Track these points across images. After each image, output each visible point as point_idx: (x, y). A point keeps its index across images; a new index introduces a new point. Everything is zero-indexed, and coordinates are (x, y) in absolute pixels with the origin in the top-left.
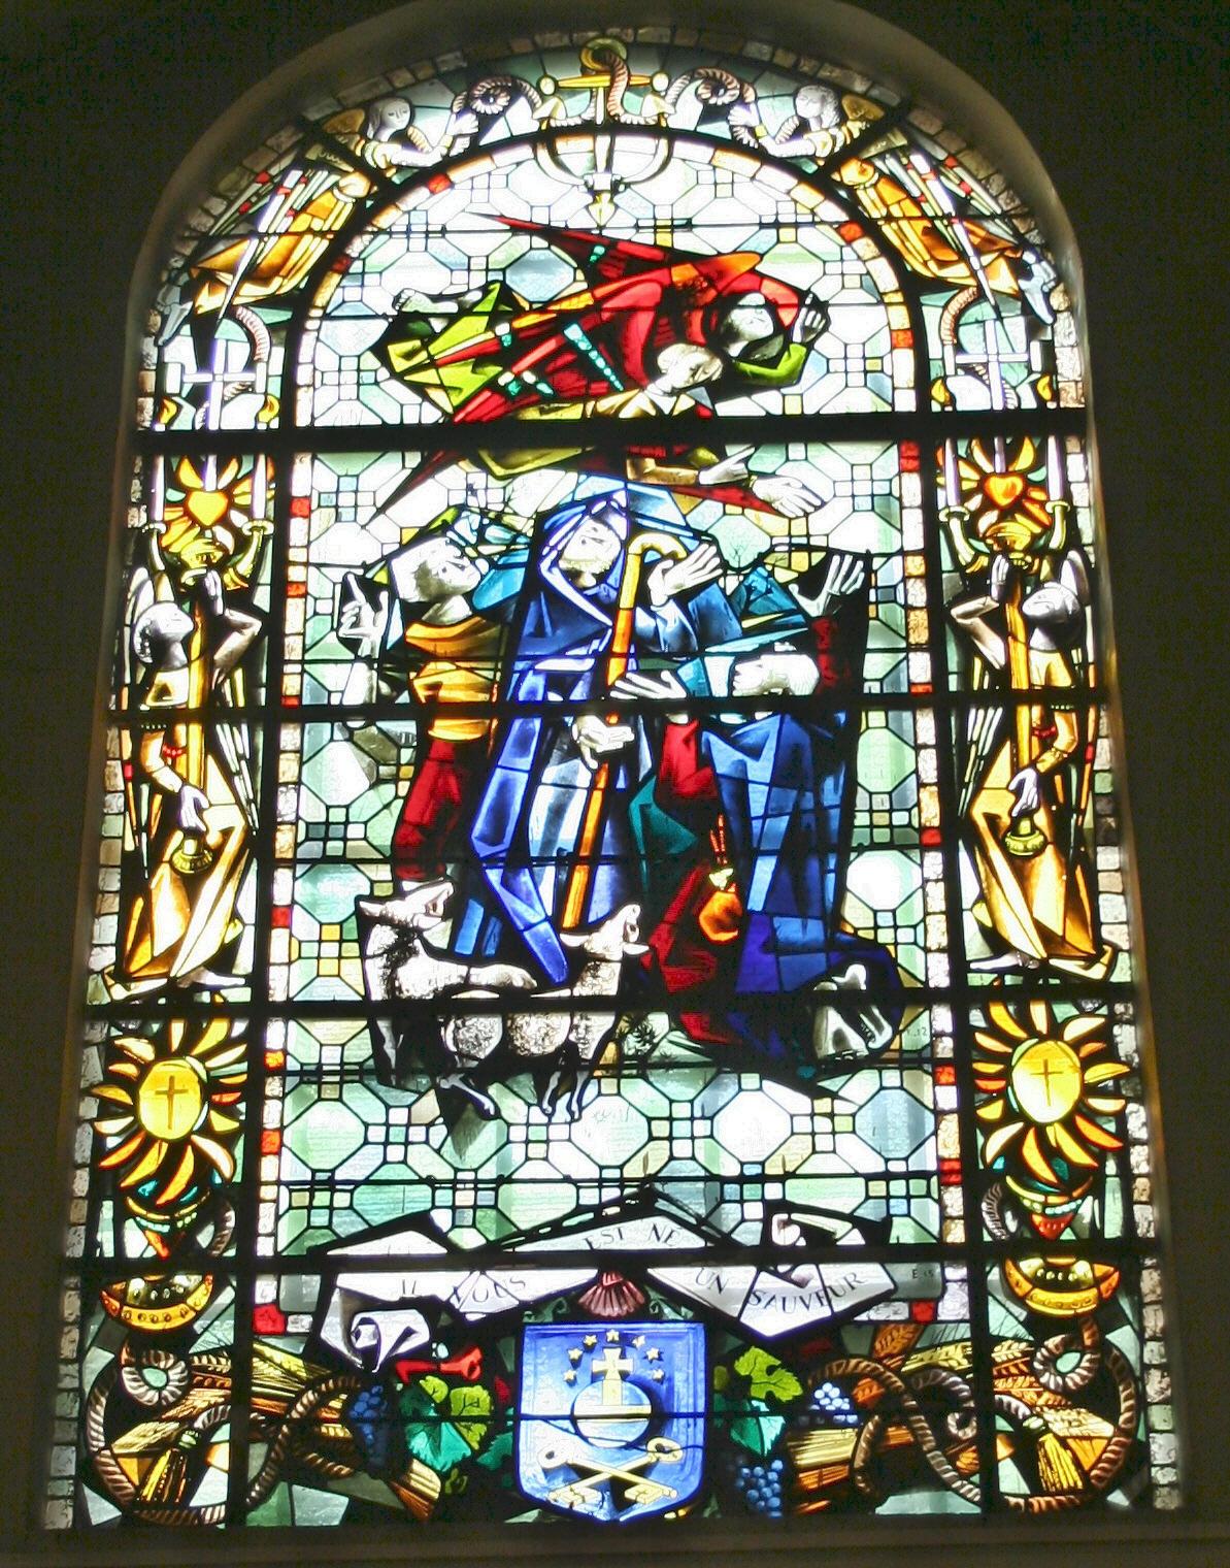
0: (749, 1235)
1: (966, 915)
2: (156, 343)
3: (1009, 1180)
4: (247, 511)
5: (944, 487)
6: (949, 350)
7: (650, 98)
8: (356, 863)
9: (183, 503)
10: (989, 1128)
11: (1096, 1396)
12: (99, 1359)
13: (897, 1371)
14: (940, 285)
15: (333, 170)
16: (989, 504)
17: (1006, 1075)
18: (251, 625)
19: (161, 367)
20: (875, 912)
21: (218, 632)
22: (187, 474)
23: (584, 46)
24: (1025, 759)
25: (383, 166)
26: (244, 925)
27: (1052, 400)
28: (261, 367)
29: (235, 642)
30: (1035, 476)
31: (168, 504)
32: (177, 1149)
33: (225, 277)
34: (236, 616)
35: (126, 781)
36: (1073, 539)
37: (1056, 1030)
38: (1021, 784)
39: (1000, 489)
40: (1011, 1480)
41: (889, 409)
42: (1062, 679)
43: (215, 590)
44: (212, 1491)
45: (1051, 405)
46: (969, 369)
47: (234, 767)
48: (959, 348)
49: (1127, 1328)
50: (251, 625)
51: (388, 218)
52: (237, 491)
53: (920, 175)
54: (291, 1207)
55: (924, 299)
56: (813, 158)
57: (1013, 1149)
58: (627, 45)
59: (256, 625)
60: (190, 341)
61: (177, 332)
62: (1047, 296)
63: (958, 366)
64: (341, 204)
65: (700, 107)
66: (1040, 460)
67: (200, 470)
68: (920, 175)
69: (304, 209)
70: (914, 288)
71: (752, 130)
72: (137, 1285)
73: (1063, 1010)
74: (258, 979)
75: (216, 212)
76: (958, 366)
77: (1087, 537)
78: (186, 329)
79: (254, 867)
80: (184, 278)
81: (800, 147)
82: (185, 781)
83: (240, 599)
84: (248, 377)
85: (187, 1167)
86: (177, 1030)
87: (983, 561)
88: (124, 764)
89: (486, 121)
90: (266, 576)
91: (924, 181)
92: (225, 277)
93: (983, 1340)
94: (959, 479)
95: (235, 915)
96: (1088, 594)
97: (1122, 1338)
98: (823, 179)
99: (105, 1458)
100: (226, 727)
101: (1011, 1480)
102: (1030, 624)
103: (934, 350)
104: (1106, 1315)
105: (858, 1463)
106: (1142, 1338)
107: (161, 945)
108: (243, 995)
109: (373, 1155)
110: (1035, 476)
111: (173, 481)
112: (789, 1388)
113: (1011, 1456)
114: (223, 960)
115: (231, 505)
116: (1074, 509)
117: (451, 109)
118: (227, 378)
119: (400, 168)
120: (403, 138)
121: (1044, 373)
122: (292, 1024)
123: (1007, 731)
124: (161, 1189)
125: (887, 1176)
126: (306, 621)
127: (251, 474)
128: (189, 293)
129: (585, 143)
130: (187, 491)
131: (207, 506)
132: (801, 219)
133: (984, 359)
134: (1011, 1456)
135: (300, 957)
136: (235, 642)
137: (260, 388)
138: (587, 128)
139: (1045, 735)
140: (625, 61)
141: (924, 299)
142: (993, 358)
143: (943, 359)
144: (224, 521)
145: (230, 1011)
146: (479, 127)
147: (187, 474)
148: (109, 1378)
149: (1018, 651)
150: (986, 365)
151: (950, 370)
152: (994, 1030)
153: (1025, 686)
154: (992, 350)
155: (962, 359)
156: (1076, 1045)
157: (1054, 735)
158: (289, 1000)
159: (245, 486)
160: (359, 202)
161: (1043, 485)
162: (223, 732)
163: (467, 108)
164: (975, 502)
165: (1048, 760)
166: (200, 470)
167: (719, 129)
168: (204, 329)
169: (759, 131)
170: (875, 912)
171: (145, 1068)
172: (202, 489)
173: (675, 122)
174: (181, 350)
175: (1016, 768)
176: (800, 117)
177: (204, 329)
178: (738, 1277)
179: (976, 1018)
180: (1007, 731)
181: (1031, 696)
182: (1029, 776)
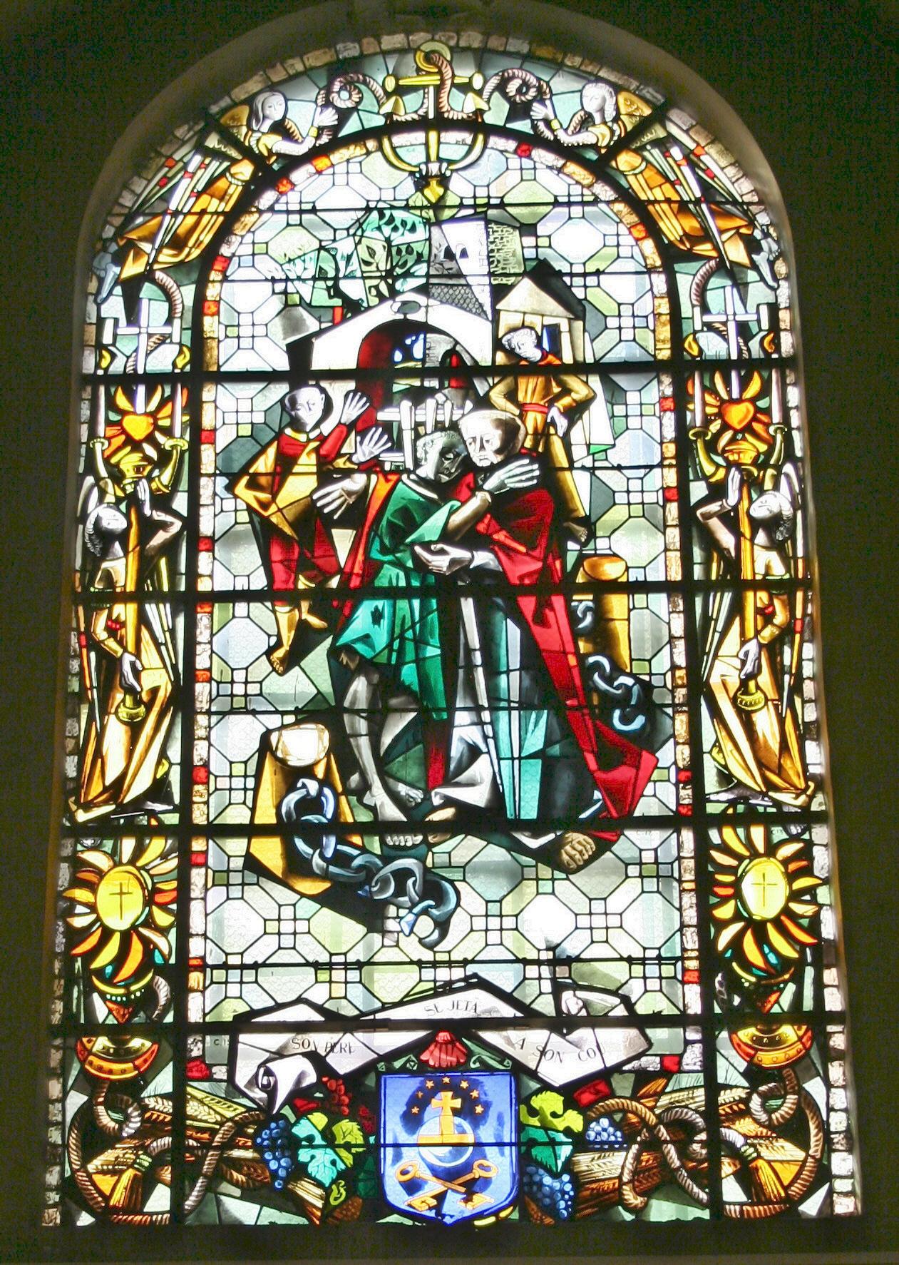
0: (545, 1006)
1: (706, 757)
2: (95, 301)
3: (734, 965)
4: (168, 432)
5: (693, 411)
6: (697, 310)
7: (471, 95)
8: (254, 713)
9: (119, 423)
10: (723, 924)
11: (794, 1130)
12: (76, 1100)
13: (651, 1109)
14: (691, 257)
15: (224, 157)
16: (726, 426)
17: (737, 885)
18: (172, 524)
19: (101, 321)
20: (553, 893)
21: (148, 528)
22: (122, 401)
23: (418, 49)
24: (750, 632)
25: (266, 153)
26: (171, 764)
27: (775, 352)
28: (177, 322)
29: (160, 538)
30: (762, 404)
31: (109, 423)
32: (126, 937)
33: (146, 247)
34: (159, 516)
35: (81, 647)
36: (789, 455)
37: (771, 850)
38: (746, 654)
39: (738, 415)
40: (732, 1192)
41: (652, 359)
42: (779, 571)
43: (144, 495)
44: (160, 1200)
45: (775, 356)
46: (709, 327)
47: (161, 640)
48: (705, 309)
49: (818, 1079)
50: (172, 524)
51: (268, 198)
52: (160, 415)
53: (675, 161)
54: (216, 789)
55: (677, 267)
56: (595, 147)
57: (737, 942)
58: (452, 49)
59: (177, 525)
60: (121, 300)
61: (110, 293)
62: (771, 264)
63: (704, 324)
64: (233, 187)
65: (506, 107)
66: (765, 391)
67: (131, 397)
68: (675, 161)
69: (204, 191)
70: (671, 256)
71: (548, 123)
72: (102, 1042)
73: (778, 834)
74: (185, 808)
75: (139, 191)
76: (704, 324)
77: (799, 453)
78: (118, 290)
79: (179, 720)
80: (113, 248)
81: (586, 138)
82: (125, 650)
83: (162, 501)
84: (167, 330)
85: (137, 948)
86: (128, 845)
87: (721, 474)
88: (80, 634)
89: (344, 115)
90: (184, 485)
91: (679, 166)
92: (146, 247)
93: (713, 1087)
94: (705, 404)
95: (163, 755)
96: (798, 503)
97: (815, 1087)
98: (601, 167)
99: (81, 1176)
100: (153, 606)
101: (732, 1192)
102: (755, 524)
103: (686, 310)
104: (800, 1067)
105: (626, 1178)
106: (829, 1086)
107: (111, 776)
108: (173, 819)
109: (271, 942)
110: (762, 404)
111: (111, 405)
112: (574, 1120)
113: (734, 1174)
114: (159, 789)
115: (156, 427)
116: (791, 429)
117: (316, 102)
118: (151, 331)
119: (280, 156)
120: (280, 128)
121: (769, 331)
122: (219, 386)
123: (737, 609)
124: (116, 972)
125: (643, 961)
126: (215, 516)
127: (171, 398)
128: (120, 260)
129: (419, 136)
130: (123, 413)
131: (138, 426)
132: (586, 199)
133: (723, 318)
134: (734, 1174)
135: (222, 511)
136: (160, 538)
137: (176, 338)
138: (422, 124)
139: (766, 615)
140: (450, 63)
141: (677, 267)
142: (731, 318)
143: (499, 759)
144: (150, 439)
145: (163, 830)
146: (338, 119)
147: (122, 401)
148: (86, 1116)
149: (746, 545)
150: (725, 324)
151: (698, 326)
152: (725, 849)
153: (749, 577)
154: (730, 311)
155: (707, 318)
156: (785, 862)
157: (773, 614)
158: (210, 824)
159: (167, 410)
160: (246, 185)
161: (767, 411)
162: (151, 609)
163: (328, 103)
164: (715, 427)
165: (768, 633)
166: (131, 397)
167: (523, 126)
168: (131, 290)
169: (555, 125)
170: (553, 893)
171: (101, 874)
172: (134, 413)
173: (489, 118)
174: (114, 307)
175: (744, 642)
176: (586, 112)
177: (131, 290)
178: (538, 1036)
179: (714, 835)
180: (737, 609)
181: (755, 585)
182: (752, 647)
